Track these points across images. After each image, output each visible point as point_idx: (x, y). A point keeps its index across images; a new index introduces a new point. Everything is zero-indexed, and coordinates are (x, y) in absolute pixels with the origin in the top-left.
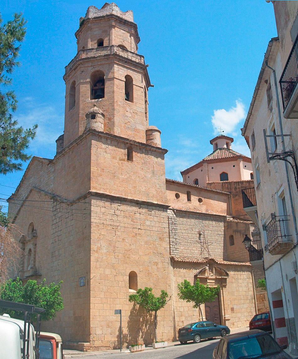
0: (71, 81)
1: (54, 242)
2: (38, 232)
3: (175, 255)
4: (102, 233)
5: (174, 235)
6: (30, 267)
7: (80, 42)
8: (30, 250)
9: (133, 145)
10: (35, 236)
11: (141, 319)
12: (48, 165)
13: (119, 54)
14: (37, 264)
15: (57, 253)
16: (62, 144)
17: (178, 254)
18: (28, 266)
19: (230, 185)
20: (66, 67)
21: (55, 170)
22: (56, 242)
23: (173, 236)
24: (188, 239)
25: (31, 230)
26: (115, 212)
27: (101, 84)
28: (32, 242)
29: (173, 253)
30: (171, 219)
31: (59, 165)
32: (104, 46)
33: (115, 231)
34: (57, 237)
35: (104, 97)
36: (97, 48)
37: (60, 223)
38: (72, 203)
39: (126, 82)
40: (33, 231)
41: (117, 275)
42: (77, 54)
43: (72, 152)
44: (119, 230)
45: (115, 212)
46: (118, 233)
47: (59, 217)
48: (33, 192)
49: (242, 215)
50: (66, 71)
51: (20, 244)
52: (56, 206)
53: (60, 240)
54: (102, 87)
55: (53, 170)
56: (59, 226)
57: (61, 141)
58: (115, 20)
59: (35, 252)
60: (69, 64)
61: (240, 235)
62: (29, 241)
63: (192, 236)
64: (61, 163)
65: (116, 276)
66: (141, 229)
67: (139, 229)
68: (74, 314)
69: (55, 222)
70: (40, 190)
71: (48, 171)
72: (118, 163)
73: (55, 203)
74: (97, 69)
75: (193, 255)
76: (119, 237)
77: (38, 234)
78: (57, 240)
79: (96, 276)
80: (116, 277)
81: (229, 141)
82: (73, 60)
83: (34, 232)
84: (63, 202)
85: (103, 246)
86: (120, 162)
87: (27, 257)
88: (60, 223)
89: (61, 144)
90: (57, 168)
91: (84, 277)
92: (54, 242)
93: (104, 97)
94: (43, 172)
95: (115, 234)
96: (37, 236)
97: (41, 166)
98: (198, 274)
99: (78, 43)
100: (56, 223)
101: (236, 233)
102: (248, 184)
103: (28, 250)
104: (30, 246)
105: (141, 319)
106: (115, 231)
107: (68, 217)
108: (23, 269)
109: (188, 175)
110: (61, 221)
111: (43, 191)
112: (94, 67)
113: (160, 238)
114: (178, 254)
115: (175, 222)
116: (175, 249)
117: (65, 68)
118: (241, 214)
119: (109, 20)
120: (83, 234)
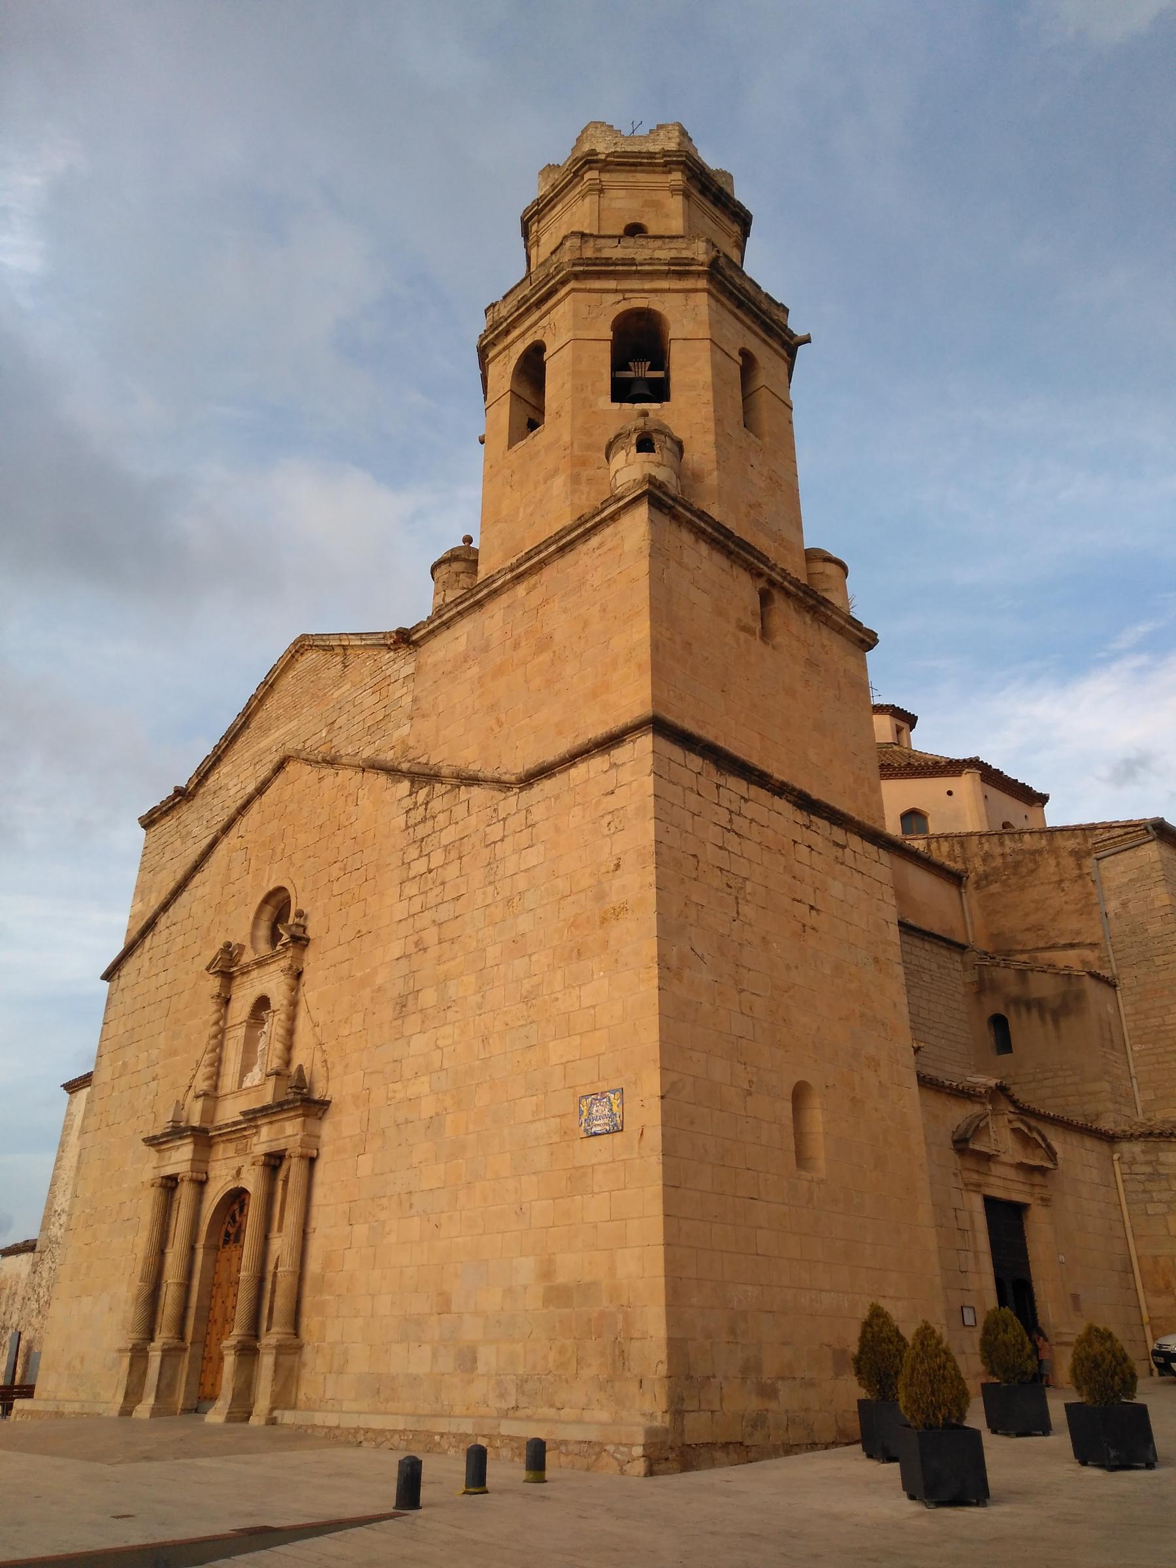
4: (695, 898)
8: (263, 1003)
10: (300, 939)
14: (300, 1057)
15: (429, 997)
18: (246, 1068)
19: (962, 844)
26: (731, 821)
31: (444, 649)
33: (736, 898)
34: (435, 930)
41: (753, 1089)
44: (748, 897)
45: (731, 821)
47: (446, 846)
49: (1022, 952)
53: (452, 941)
60: (505, 297)
61: (1042, 1018)
65: (750, 1094)
66: (818, 911)
67: (812, 907)
68: (547, 1272)
74: (638, 302)
76: (750, 924)
78: (431, 936)
80: (749, 1098)
81: (906, 726)
87: (241, 1032)
88: (449, 868)
90: (430, 661)
91: (614, 1092)
92: (412, 949)
94: (348, 686)
95: (738, 913)
100: (430, 871)
101: (1023, 1010)
102: (1044, 842)
103: (251, 1000)
107: (502, 840)
110: (460, 858)
112: (628, 295)
113: (876, 960)
118: (1019, 947)
120: (601, 896)
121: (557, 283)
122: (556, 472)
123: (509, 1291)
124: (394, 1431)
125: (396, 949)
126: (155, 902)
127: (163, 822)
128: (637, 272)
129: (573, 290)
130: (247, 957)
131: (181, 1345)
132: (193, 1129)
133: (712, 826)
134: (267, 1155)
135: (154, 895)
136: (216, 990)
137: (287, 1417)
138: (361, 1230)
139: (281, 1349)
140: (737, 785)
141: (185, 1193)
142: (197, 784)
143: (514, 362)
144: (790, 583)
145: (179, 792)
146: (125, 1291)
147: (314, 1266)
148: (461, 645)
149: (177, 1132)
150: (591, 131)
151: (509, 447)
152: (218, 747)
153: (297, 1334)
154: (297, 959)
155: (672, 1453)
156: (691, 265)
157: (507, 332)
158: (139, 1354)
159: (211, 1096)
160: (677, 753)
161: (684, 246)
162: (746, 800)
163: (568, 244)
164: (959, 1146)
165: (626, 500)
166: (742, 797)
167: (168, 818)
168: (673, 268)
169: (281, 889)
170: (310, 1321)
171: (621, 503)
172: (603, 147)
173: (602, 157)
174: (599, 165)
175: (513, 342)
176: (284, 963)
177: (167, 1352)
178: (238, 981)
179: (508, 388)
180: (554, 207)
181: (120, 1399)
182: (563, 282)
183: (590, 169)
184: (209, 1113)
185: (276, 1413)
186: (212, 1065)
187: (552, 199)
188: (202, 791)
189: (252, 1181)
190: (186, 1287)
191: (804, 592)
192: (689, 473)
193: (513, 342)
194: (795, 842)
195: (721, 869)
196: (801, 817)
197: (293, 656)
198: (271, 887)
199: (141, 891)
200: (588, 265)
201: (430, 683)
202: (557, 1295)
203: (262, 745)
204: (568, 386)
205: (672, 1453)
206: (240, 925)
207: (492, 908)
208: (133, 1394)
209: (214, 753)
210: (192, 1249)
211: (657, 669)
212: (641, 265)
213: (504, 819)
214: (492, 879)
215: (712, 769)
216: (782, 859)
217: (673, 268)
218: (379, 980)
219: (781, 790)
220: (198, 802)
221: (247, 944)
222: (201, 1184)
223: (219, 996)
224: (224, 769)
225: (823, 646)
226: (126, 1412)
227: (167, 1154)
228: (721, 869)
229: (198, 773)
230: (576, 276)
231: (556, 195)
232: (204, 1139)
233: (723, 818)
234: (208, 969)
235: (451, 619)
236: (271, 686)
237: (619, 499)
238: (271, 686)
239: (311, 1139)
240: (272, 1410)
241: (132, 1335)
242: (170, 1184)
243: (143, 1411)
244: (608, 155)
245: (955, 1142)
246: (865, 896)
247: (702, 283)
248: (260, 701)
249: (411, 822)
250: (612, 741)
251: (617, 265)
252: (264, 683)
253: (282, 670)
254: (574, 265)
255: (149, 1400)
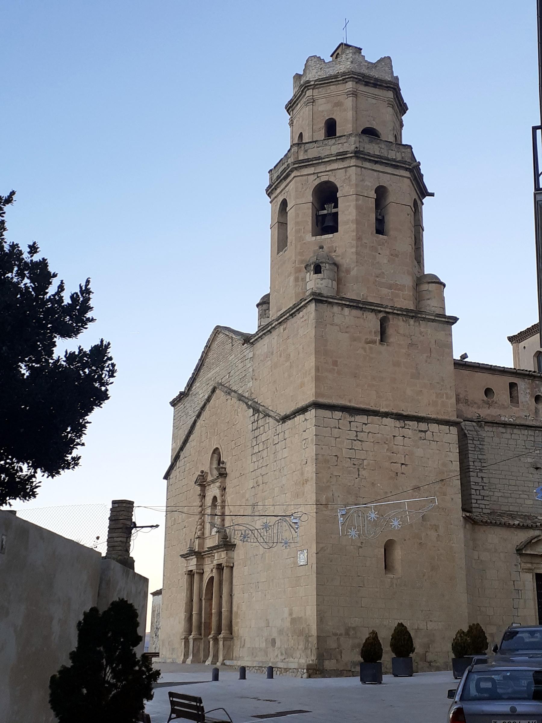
0: (280, 199)
1: (255, 485)
2: (228, 466)
3: (482, 509)
5: (478, 470)
6: (215, 530)
7: (295, 122)
8: (215, 498)
9: (209, 513)
10: (223, 474)
11: (109, 635)
12: (243, 345)
13: (364, 148)
16: (267, 311)
17: (487, 507)
20: (271, 170)
21: (254, 355)
22: (259, 485)
23: (477, 472)
24: (511, 477)
25: (215, 465)
26: (357, 436)
27: (333, 204)
28: (218, 484)
29: (477, 505)
30: (473, 440)
31: (262, 346)
32: (338, 135)
35: (337, 231)
36: (324, 140)
37: (265, 451)
38: (285, 419)
39: (376, 199)
40: (219, 465)
42: (289, 151)
43: (284, 330)
45: (357, 436)
46: (363, 473)
48: (217, 391)
50: (271, 179)
51: (197, 486)
52: (257, 421)
53: (266, 483)
54: (334, 210)
55: (251, 355)
56: (263, 458)
57: (265, 307)
58: (357, 80)
59: (223, 501)
60: (275, 167)
62: (213, 482)
63: (519, 472)
64: (266, 345)
66: (406, 465)
67: (403, 464)
68: (291, 614)
69: (256, 450)
70: (229, 391)
71: (242, 356)
72: (362, 348)
73: (257, 415)
74: (324, 179)
75: (521, 508)
76: (365, 478)
77: (227, 470)
78: (260, 482)
79: (326, 548)
82: (281, 160)
83: (221, 465)
84: (269, 416)
85: (336, 495)
86: (367, 346)
89: (265, 311)
92: (255, 485)
93: (337, 231)
94: (233, 356)
95: (359, 475)
96: (226, 474)
97: (231, 344)
98: (523, 548)
99: (291, 124)
100: (259, 452)
103: (212, 497)
104: (213, 491)
105: (109, 635)
106: (358, 469)
108: (203, 534)
109: (522, 344)
111: (235, 392)
112: (319, 175)
114: (487, 507)
115: (480, 446)
116: (480, 497)
117: (269, 172)
119: (346, 82)
120: (302, 474)
121: (289, 171)
122: (289, 275)
123: (282, 620)
124: (253, 667)
125: (251, 484)
126: (180, 444)
127: (179, 405)
128: (322, 162)
129: (295, 177)
130: (209, 478)
131: (200, 637)
132: (195, 552)
133: (346, 441)
134: (217, 565)
135: (178, 441)
136: (199, 492)
137: (228, 662)
138: (246, 595)
139: (225, 639)
140: (362, 419)
141: (196, 577)
142: (188, 390)
143: (279, 203)
144: (398, 310)
145: (181, 394)
146: (182, 615)
147: (235, 609)
148: (265, 349)
149: (192, 553)
150: (310, 59)
151: (278, 253)
152: (193, 374)
153: (231, 634)
154: (223, 482)
155: (315, 671)
156: (347, 154)
157: (275, 189)
158: (186, 640)
159: (202, 537)
160: (327, 413)
161: (345, 141)
162: (366, 424)
163: (292, 150)
164: (518, 552)
165: (307, 301)
166: (364, 424)
167: (180, 403)
168: (338, 157)
169: (217, 448)
170: (235, 629)
171: (306, 301)
172: (313, 76)
173: (312, 83)
174: (312, 87)
175: (278, 195)
176: (218, 484)
177: (195, 640)
178: (207, 488)
179: (276, 221)
180: (297, 104)
181: (183, 657)
182: (292, 171)
183: (308, 89)
184: (201, 545)
185: (225, 661)
186: (201, 524)
187: (295, 102)
188: (191, 393)
189: (215, 574)
190: (200, 614)
191: (406, 312)
192: (344, 270)
193: (278, 195)
194: (394, 436)
195: (350, 458)
196: (398, 424)
197: (215, 335)
198: (215, 448)
199: (175, 437)
200: (300, 163)
201: (257, 364)
202: (294, 621)
203: (209, 375)
204: (294, 230)
205: (315, 671)
206: (205, 464)
207: (276, 472)
208: (186, 655)
209: (192, 377)
210: (201, 600)
211: (318, 379)
212: (324, 158)
213: (278, 434)
214: (275, 459)
215: (347, 415)
216: (386, 446)
217: (338, 157)
218: (247, 496)
219: (386, 415)
220: (189, 398)
221: (209, 472)
222: (201, 574)
223: (200, 494)
224: (197, 384)
225: (421, 333)
226: (184, 662)
227: (189, 561)
228: (350, 458)
229: (188, 385)
230: (296, 169)
231: (297, 100)
232: (200, 555)
233: (352, 435)
234: (195, 483)
235: (262, 336)
236: (209, 347)
237: (305, 300)
238: (209, 347)
239: (230, 558)
240: (224, 660)
241: (184, 633)
242: (191, 574)
243: (189, 661)
244: (316, 81)
245: (517, 550)
246: (438, 452)
247: (353, 162)
248: (206, 354)
249: (254, 428)
250: (303, 410)
251: (313, 161)
252: (206, 346)
253: (212, 341)
254: (294, 164)
255: (191, 657)
